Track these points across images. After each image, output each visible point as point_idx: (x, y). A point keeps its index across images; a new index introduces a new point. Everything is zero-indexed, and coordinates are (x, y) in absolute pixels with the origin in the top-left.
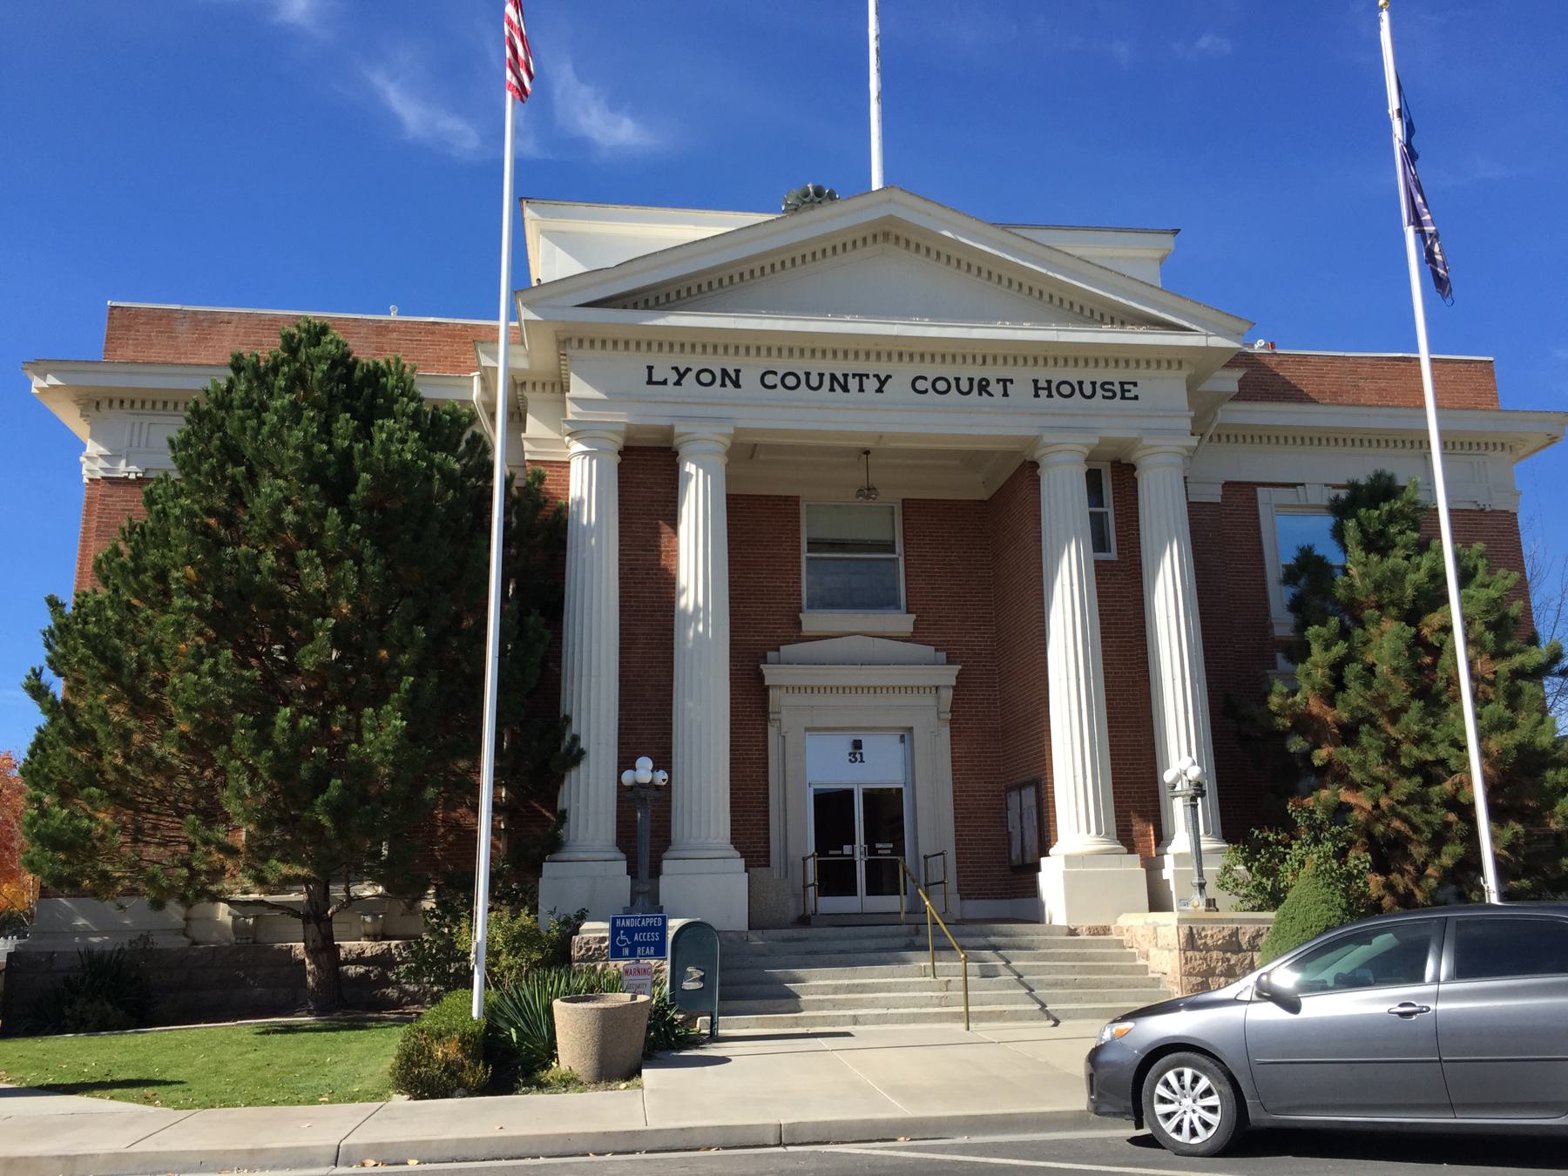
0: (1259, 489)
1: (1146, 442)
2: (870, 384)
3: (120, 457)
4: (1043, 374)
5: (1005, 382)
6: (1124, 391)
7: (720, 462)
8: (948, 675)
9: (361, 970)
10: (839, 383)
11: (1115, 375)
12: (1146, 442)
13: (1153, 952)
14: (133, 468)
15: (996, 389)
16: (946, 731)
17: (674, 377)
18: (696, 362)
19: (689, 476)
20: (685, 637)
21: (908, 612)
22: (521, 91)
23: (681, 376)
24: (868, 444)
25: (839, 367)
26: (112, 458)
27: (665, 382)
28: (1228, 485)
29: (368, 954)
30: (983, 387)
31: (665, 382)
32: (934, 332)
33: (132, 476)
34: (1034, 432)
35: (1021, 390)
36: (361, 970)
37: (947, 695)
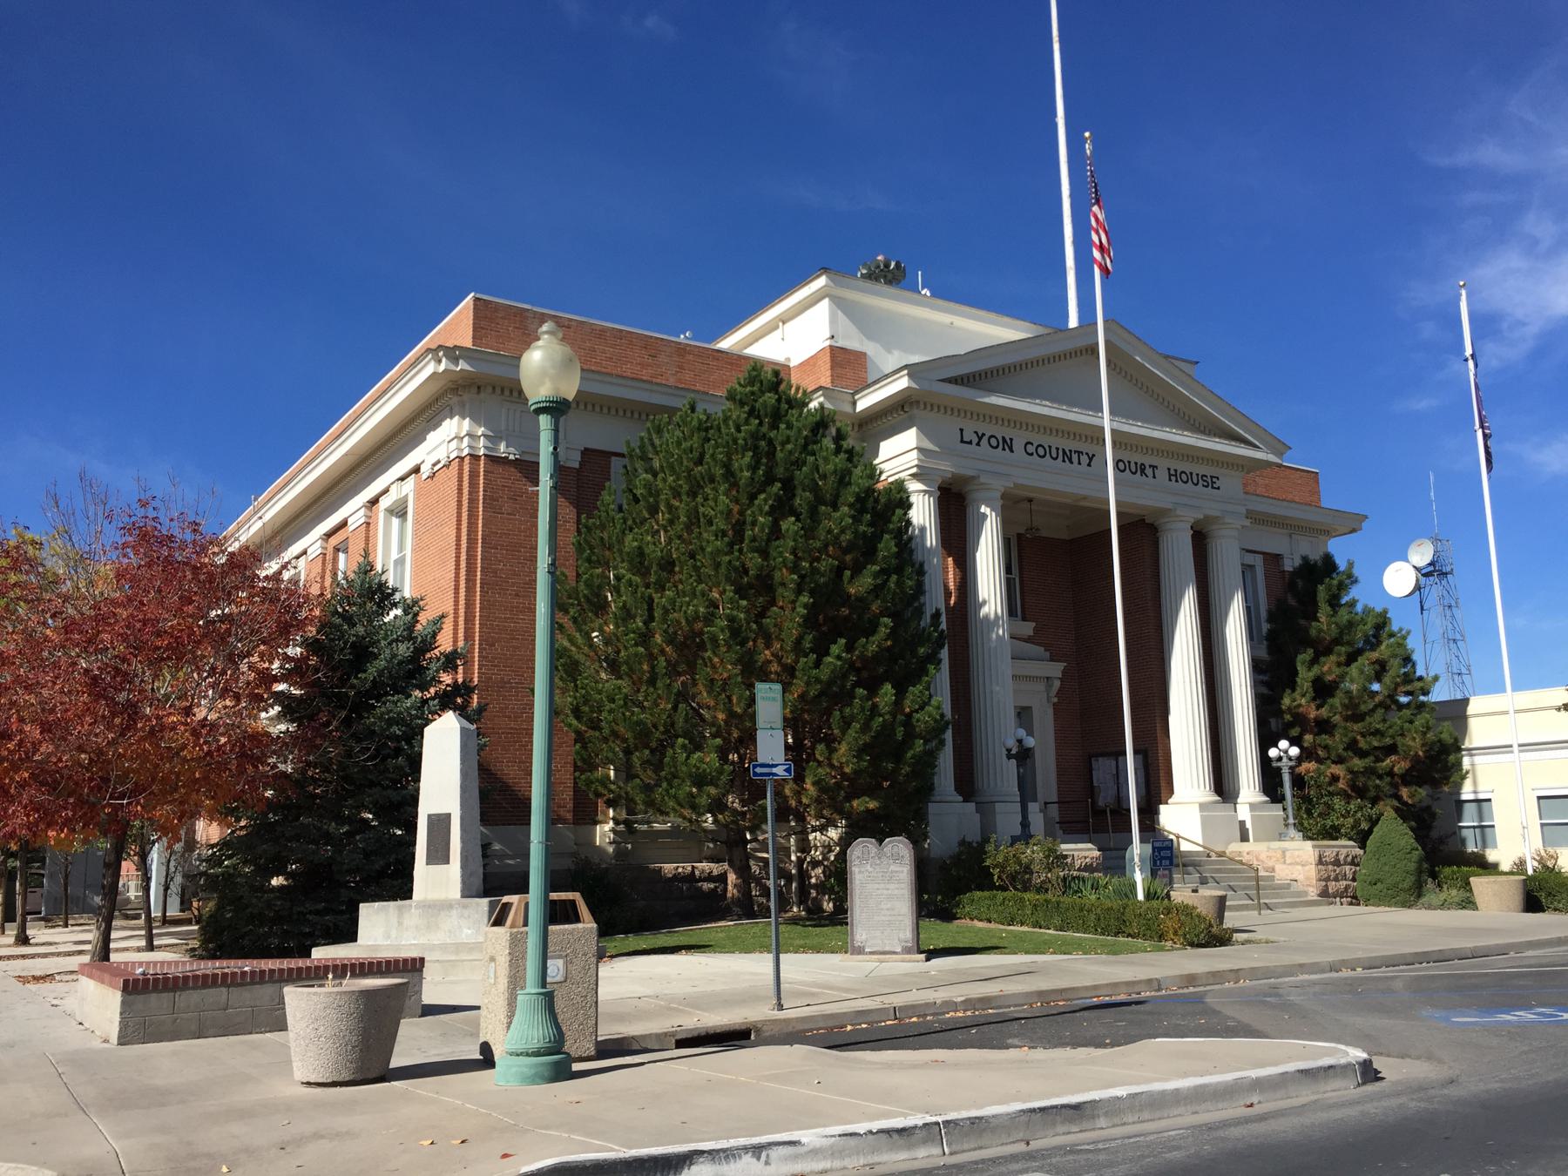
0: (613, 459)
1: (982, 480)
2: (1085, 459)
3: (501, 439)
4: (1037, 439)
5: (1154, 467)
6: (1211, 482)
7: (999, 503)
8: (1056, 669)
9: (712, 886)
10: (1067, 456)
11: (1207, 470)
12: (982, 480)
13: (1278, 867)
14: (512, 450)
15: (1149, 471)
16: (1050, 711)
17: (975, 440)
18: (988, 429)
19: (984, 516)
20: (990, 639)
21: (1024, 619)
22: (1105, 271)
23: (980, 439)
24: (1032, 495)
25: (1069, 445)
26: (493, 439)
27: (970, 443)
28: (586, 452)
29: (715, 873)
30: (1142, 469)
31: (970, 443)
32: (1157, 434)
33: (512, 457)
34: (970, 473)
35: (1162, 474)
36: (712, 886)
37: (1057, 684)
